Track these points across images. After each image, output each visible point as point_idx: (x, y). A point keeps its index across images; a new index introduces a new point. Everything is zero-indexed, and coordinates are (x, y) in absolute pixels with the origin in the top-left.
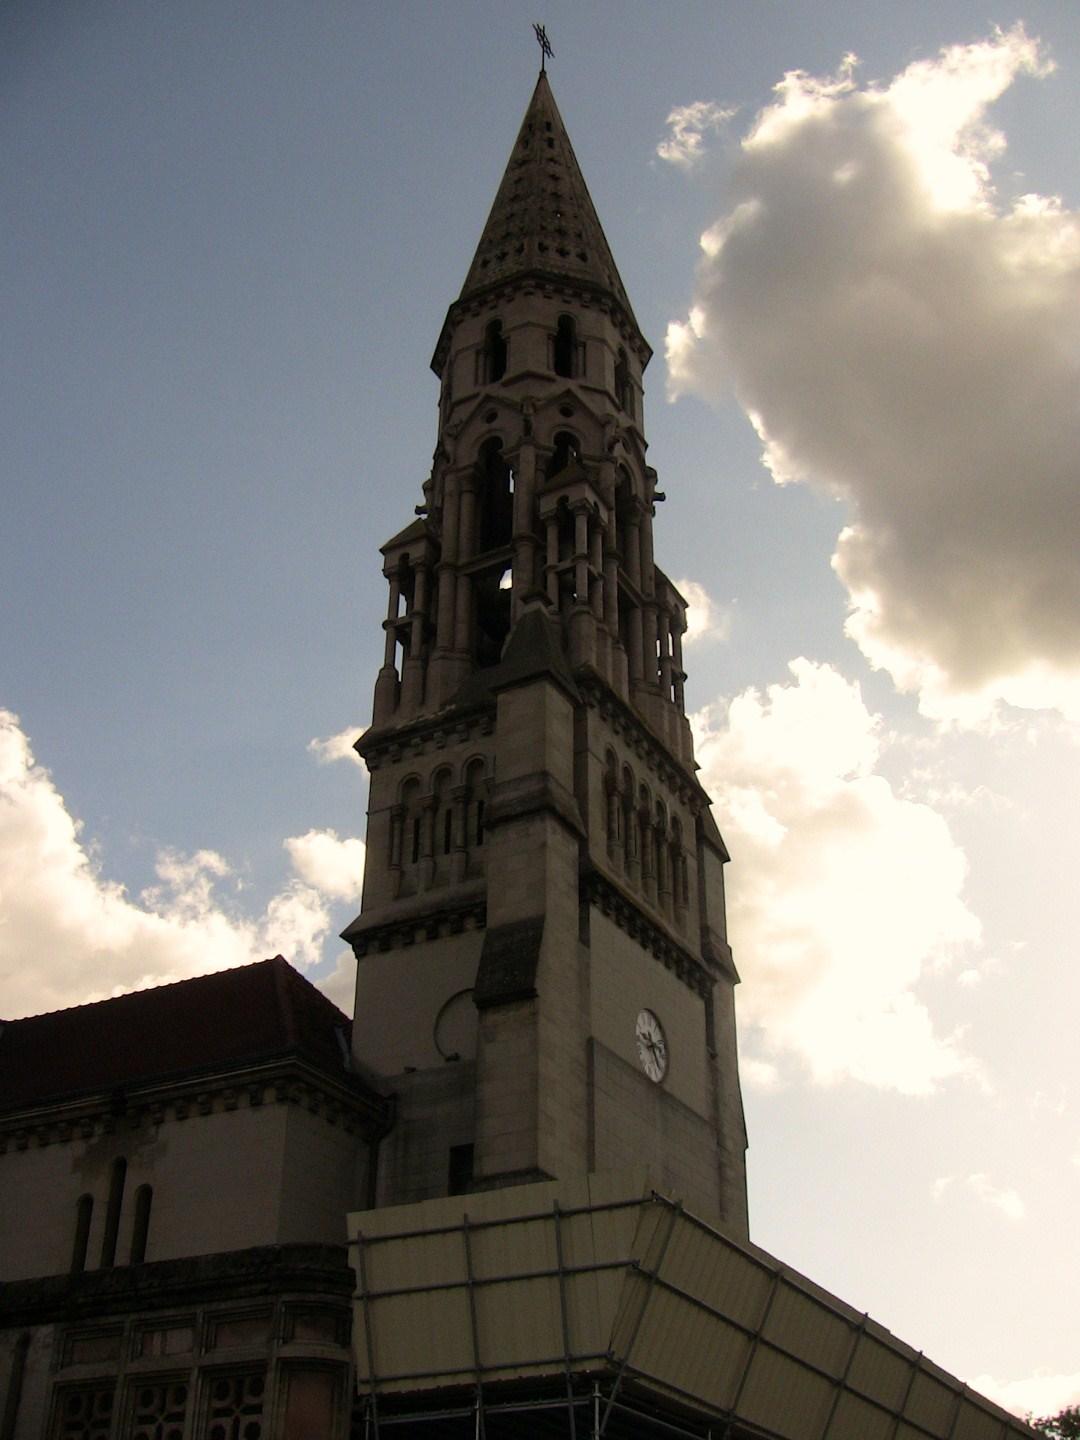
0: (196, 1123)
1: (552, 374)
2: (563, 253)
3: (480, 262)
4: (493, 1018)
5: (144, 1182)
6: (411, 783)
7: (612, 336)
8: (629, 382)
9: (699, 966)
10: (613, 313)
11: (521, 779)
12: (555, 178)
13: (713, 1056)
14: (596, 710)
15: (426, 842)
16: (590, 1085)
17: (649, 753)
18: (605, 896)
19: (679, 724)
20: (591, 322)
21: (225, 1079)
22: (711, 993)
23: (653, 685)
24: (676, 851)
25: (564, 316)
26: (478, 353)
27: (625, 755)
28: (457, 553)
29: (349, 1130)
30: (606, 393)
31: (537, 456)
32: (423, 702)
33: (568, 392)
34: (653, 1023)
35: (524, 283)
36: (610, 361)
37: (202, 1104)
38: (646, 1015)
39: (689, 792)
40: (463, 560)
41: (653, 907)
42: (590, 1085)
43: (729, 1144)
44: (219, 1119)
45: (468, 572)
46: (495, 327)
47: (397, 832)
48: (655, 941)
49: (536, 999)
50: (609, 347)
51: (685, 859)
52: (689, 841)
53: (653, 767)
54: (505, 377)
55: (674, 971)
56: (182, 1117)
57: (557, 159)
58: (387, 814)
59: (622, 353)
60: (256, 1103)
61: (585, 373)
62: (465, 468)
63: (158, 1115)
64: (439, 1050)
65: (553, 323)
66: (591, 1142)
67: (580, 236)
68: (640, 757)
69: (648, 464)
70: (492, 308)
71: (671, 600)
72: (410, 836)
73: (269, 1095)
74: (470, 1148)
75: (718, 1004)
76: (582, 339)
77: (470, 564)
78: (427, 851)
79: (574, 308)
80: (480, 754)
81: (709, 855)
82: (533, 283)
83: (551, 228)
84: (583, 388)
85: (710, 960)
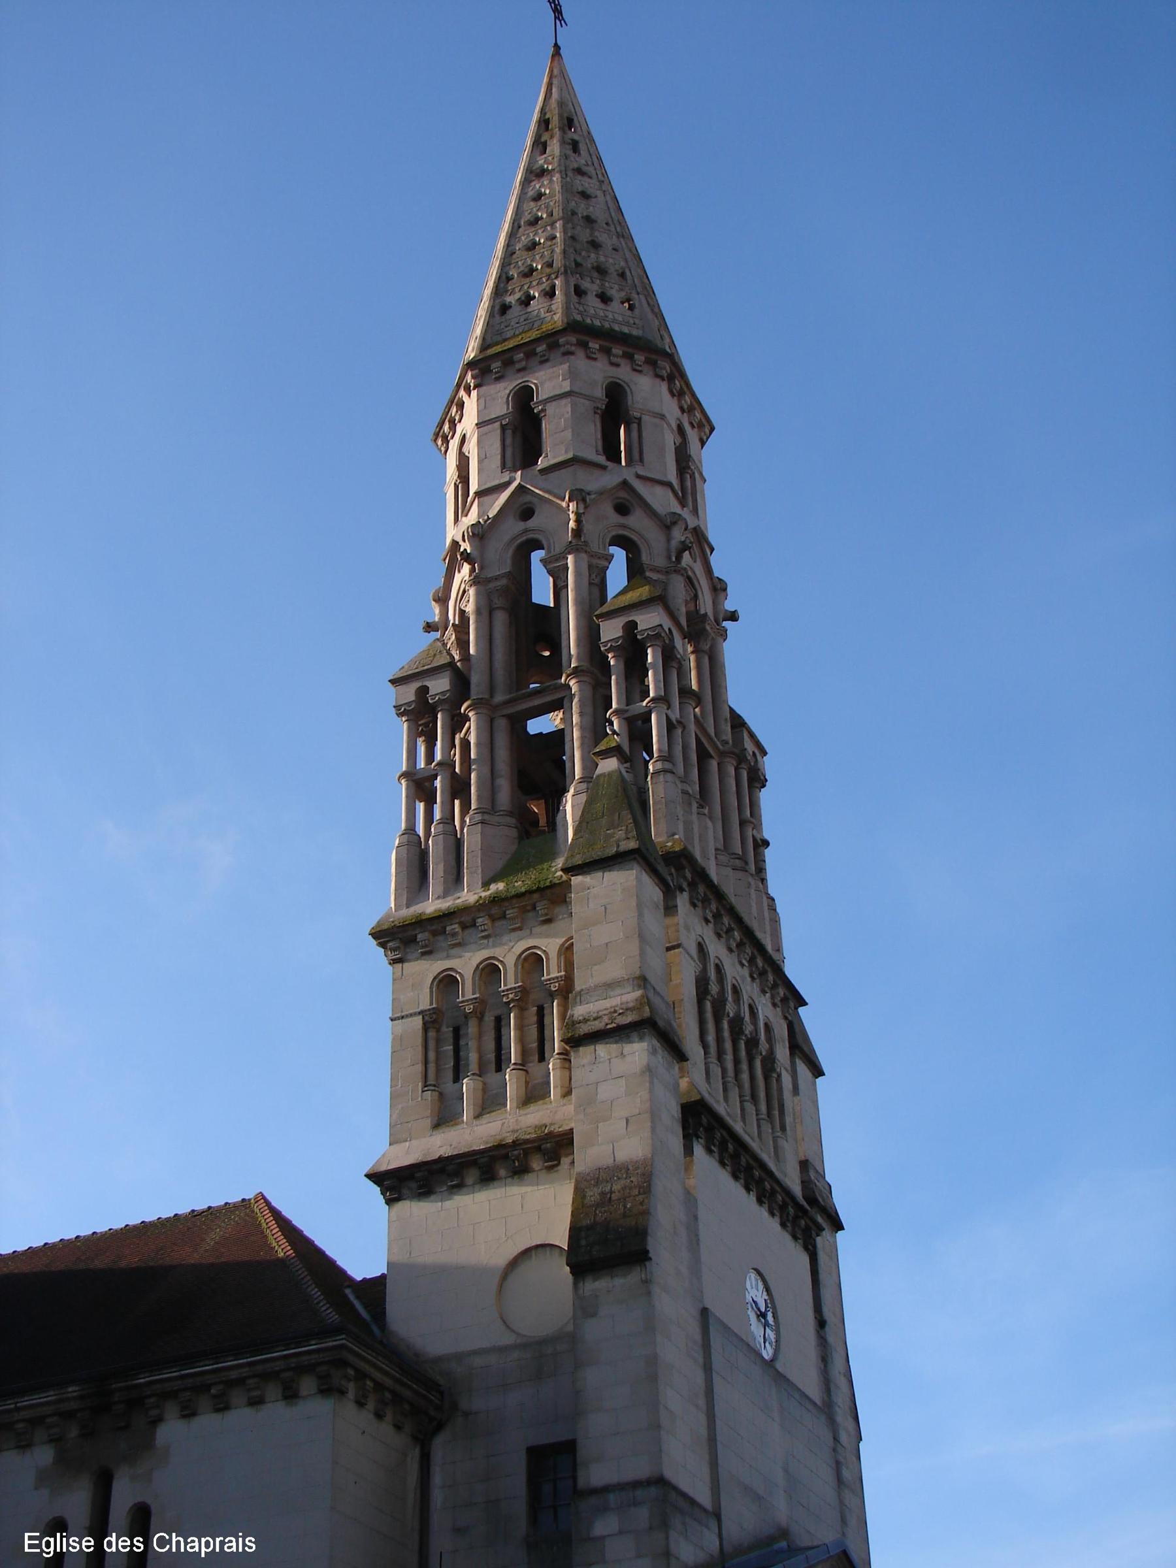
0: (207, 1422)
1: (602, 459)
2: (604, 298)
3: (497, 308)
4: (591, 1286)
5: (139, 1499)
6: (447, 982)
7: (671, 408)
8: (689, 468)
9: (805, 1212)
10: (670, 379)
11: (610, 986)
12: (585, 195)
13: (821, 1323)
14: (686, 895)
15: (473, 1057)
16: (708, 1368)
17: (740, 945)
18: (709, 1130)
19: (765, 904)
20: (646, 391)
21: (250, 1364)
22: (815, 1246)
23: (734, 855)
24: (769, 1062)
25: (612, 383)
26: (503, 428)
27: (717, 949)
28: (492, 689)
29: (398, 1427)
30: (669, 485)
31: (590, 566)
32: (458, 879)
33: (625, 484)
34: (761, 1286)
35: (562, 341)
36: (670, 440)
37: (215, 1396)
38: (753, 1275)
39: (781, 991)
40: (499, 698)
41: (752, 1139)
42: (708, 1368)
43: (843, 1437)
44: (241, 1417)
45: (506, 712)
46: (524, 396)
47: (432, 1044)
48: (759, 1182)
49: (647, 1263)
50: (669, 425)
51: (779, 1076)
52: (782, 1053)
53: (744, 962)
54: (541, 463)
55: (777, 1219)
56: (189, 1413)
57: (585, 169)
58: (418, 1020)
59: (681, 430)
60: (291, 1395)
61: (641, 460)
62: (497, 578)
63: (154, 1413)
64: (508, 1327)
65: (600, 393)
66: (712, 1440)
67: (622, 275)
68: (730, 950)
69: (717, 573)
70: (519, 370)
71: (749, 746)
72: (449, 1048)
73: (308, 1385)
74: (569, 1448)
75: (822, 1257)
76: (637, 415)
77: (506, 703)
78: (474, 1066)
79: (623, 372)
80: (539, 948)
81: (802, 1069)
82: (573, 339)
83: (588, 264)
84: (638, 476)
85: (812, 1200)
